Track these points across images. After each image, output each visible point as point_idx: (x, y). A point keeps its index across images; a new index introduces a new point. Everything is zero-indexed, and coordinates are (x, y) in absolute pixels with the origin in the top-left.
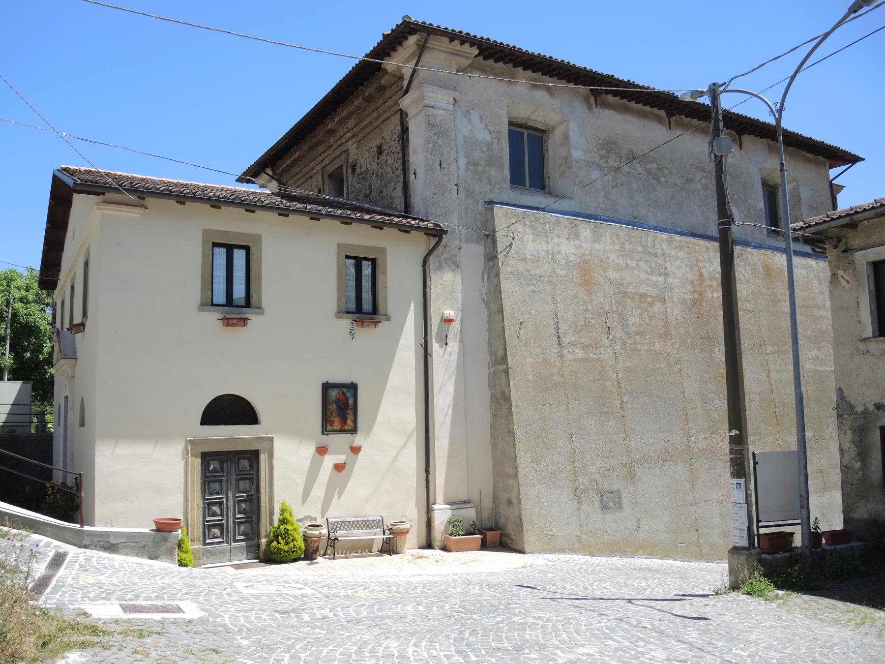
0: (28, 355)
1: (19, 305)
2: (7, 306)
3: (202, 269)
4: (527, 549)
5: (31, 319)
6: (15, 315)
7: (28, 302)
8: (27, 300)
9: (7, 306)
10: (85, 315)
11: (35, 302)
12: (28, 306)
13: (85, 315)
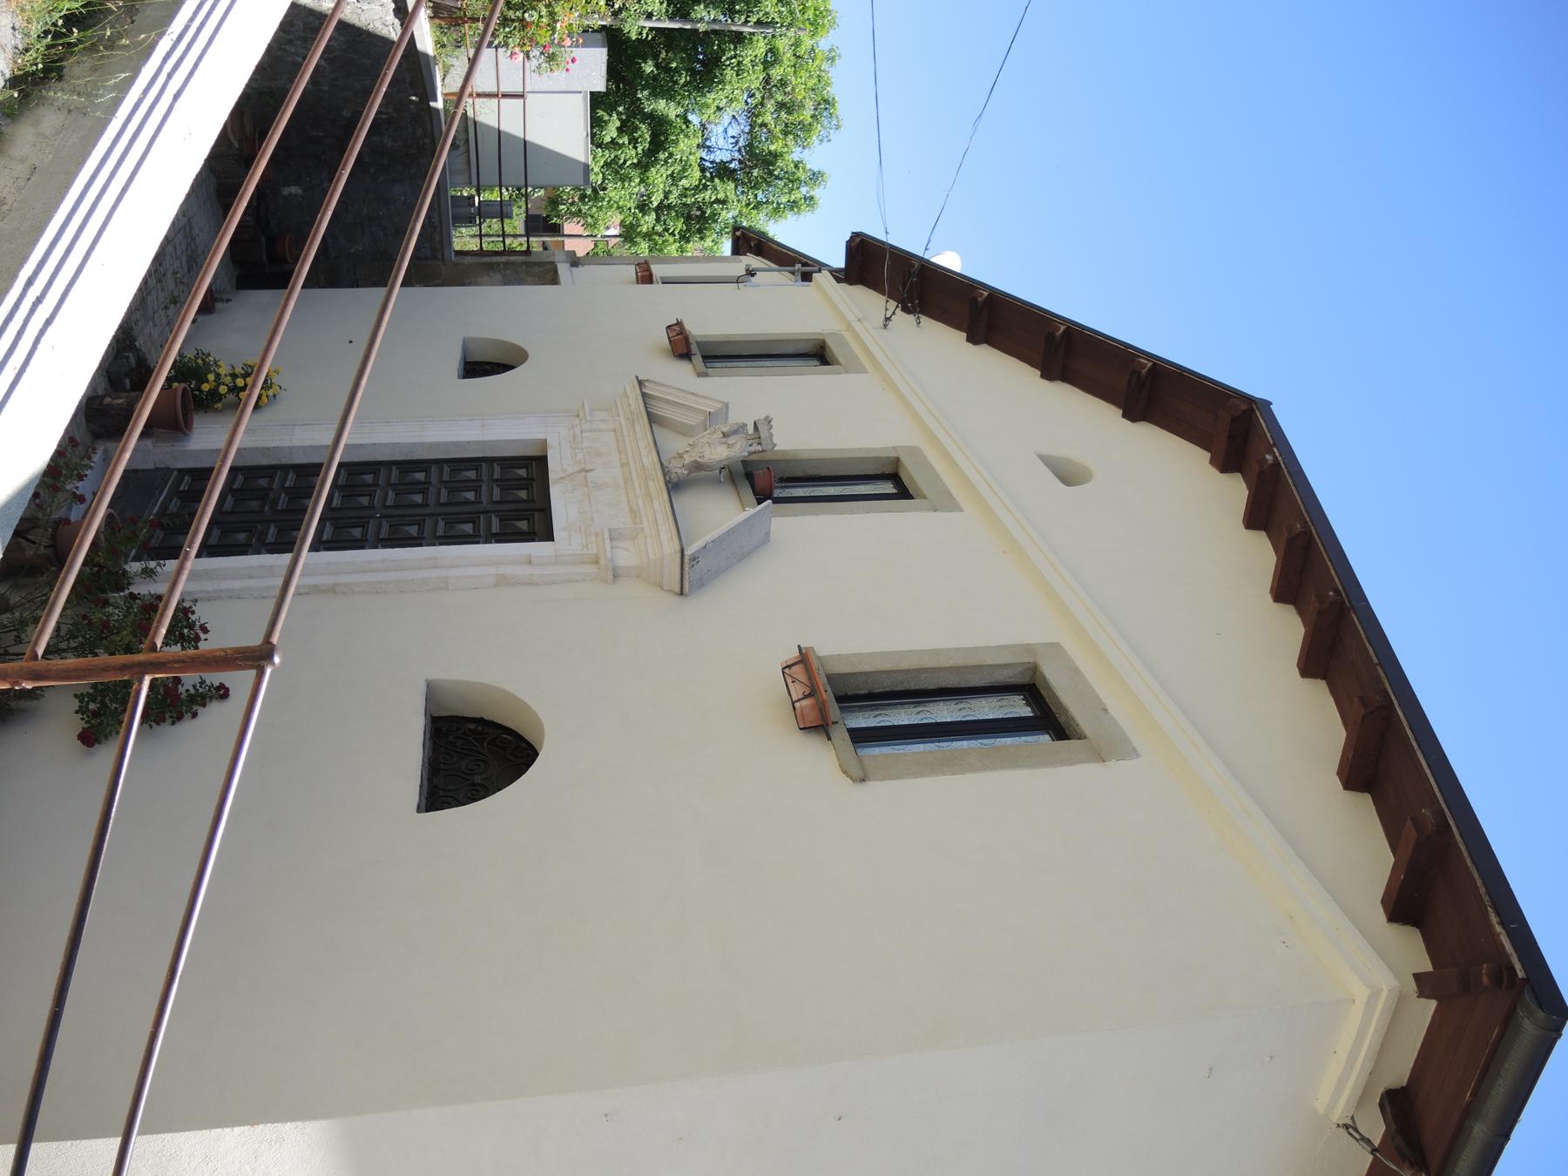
0: (649, 68)
1: (760, 48)
2: (759, 23)
3: (252, 79)
4: (149, 443)
5: (729, 73)
6: (738, 39)
7: (767, 65)
8: (773, 64)
9: (759, 23)
10: (666, 281)
11: (767, 80)
12: (761, 67)
13: (666, 281)
